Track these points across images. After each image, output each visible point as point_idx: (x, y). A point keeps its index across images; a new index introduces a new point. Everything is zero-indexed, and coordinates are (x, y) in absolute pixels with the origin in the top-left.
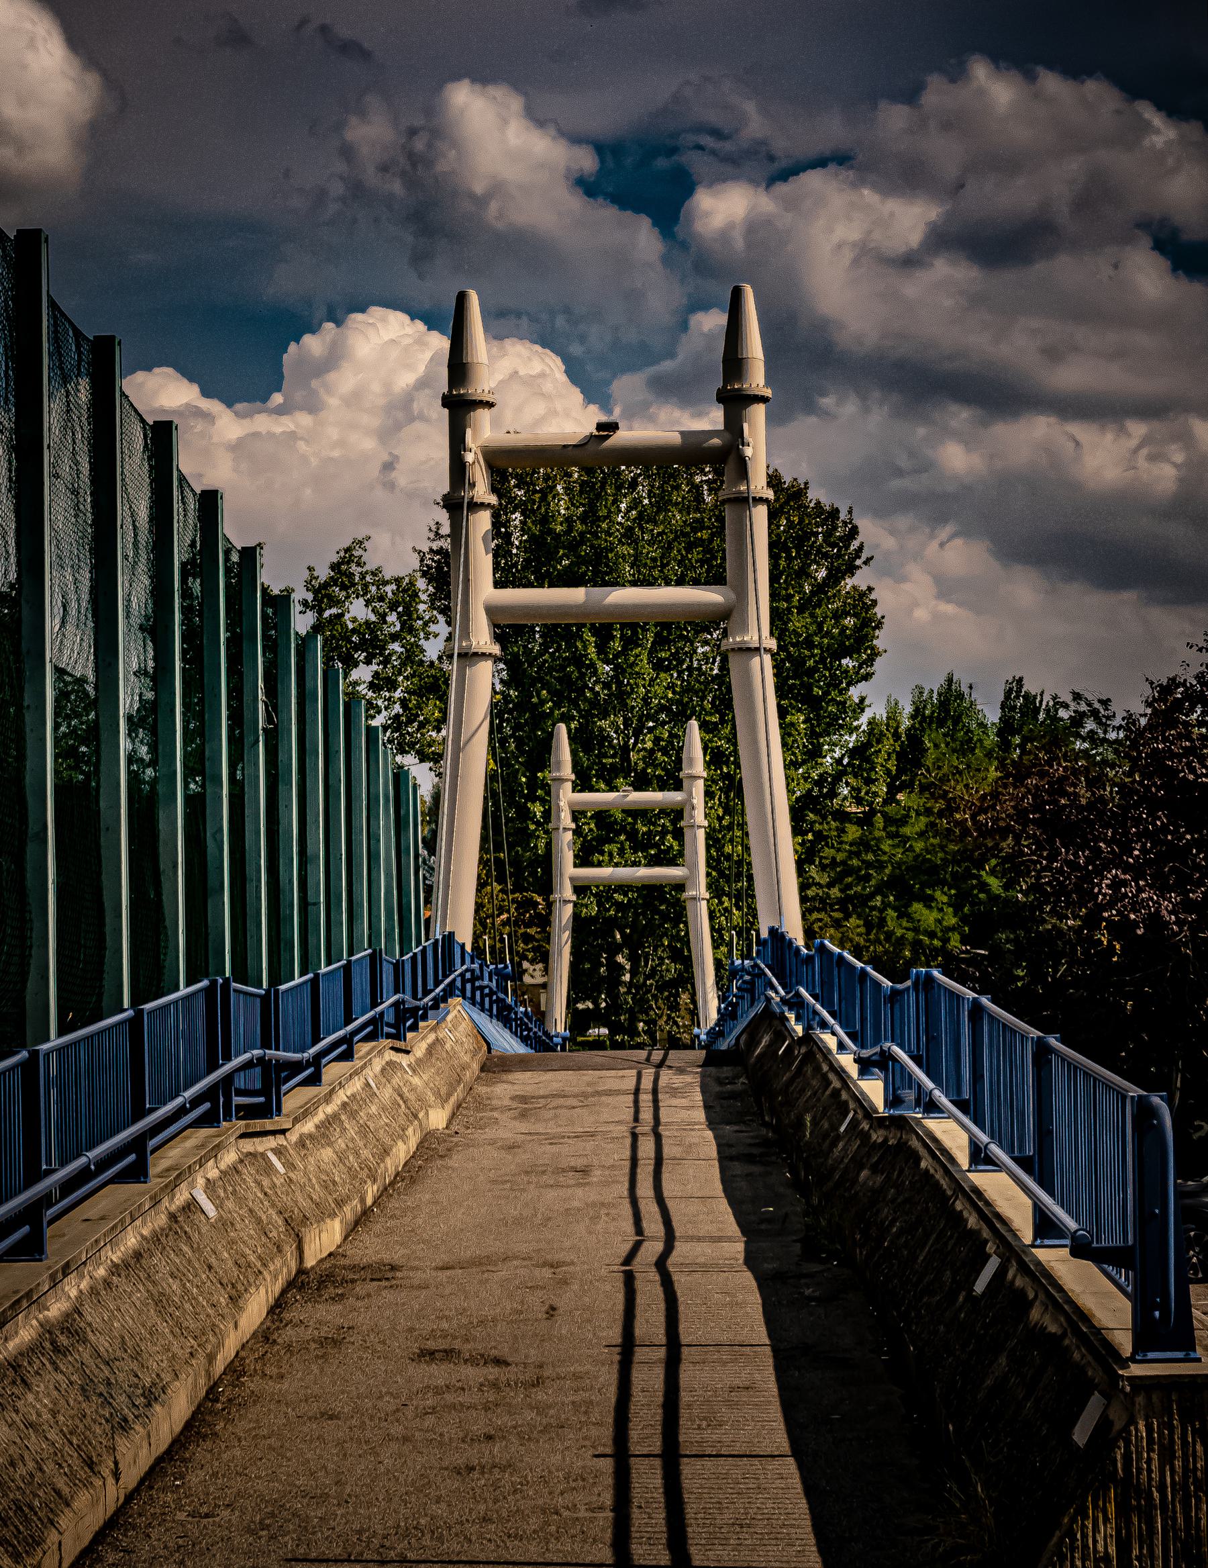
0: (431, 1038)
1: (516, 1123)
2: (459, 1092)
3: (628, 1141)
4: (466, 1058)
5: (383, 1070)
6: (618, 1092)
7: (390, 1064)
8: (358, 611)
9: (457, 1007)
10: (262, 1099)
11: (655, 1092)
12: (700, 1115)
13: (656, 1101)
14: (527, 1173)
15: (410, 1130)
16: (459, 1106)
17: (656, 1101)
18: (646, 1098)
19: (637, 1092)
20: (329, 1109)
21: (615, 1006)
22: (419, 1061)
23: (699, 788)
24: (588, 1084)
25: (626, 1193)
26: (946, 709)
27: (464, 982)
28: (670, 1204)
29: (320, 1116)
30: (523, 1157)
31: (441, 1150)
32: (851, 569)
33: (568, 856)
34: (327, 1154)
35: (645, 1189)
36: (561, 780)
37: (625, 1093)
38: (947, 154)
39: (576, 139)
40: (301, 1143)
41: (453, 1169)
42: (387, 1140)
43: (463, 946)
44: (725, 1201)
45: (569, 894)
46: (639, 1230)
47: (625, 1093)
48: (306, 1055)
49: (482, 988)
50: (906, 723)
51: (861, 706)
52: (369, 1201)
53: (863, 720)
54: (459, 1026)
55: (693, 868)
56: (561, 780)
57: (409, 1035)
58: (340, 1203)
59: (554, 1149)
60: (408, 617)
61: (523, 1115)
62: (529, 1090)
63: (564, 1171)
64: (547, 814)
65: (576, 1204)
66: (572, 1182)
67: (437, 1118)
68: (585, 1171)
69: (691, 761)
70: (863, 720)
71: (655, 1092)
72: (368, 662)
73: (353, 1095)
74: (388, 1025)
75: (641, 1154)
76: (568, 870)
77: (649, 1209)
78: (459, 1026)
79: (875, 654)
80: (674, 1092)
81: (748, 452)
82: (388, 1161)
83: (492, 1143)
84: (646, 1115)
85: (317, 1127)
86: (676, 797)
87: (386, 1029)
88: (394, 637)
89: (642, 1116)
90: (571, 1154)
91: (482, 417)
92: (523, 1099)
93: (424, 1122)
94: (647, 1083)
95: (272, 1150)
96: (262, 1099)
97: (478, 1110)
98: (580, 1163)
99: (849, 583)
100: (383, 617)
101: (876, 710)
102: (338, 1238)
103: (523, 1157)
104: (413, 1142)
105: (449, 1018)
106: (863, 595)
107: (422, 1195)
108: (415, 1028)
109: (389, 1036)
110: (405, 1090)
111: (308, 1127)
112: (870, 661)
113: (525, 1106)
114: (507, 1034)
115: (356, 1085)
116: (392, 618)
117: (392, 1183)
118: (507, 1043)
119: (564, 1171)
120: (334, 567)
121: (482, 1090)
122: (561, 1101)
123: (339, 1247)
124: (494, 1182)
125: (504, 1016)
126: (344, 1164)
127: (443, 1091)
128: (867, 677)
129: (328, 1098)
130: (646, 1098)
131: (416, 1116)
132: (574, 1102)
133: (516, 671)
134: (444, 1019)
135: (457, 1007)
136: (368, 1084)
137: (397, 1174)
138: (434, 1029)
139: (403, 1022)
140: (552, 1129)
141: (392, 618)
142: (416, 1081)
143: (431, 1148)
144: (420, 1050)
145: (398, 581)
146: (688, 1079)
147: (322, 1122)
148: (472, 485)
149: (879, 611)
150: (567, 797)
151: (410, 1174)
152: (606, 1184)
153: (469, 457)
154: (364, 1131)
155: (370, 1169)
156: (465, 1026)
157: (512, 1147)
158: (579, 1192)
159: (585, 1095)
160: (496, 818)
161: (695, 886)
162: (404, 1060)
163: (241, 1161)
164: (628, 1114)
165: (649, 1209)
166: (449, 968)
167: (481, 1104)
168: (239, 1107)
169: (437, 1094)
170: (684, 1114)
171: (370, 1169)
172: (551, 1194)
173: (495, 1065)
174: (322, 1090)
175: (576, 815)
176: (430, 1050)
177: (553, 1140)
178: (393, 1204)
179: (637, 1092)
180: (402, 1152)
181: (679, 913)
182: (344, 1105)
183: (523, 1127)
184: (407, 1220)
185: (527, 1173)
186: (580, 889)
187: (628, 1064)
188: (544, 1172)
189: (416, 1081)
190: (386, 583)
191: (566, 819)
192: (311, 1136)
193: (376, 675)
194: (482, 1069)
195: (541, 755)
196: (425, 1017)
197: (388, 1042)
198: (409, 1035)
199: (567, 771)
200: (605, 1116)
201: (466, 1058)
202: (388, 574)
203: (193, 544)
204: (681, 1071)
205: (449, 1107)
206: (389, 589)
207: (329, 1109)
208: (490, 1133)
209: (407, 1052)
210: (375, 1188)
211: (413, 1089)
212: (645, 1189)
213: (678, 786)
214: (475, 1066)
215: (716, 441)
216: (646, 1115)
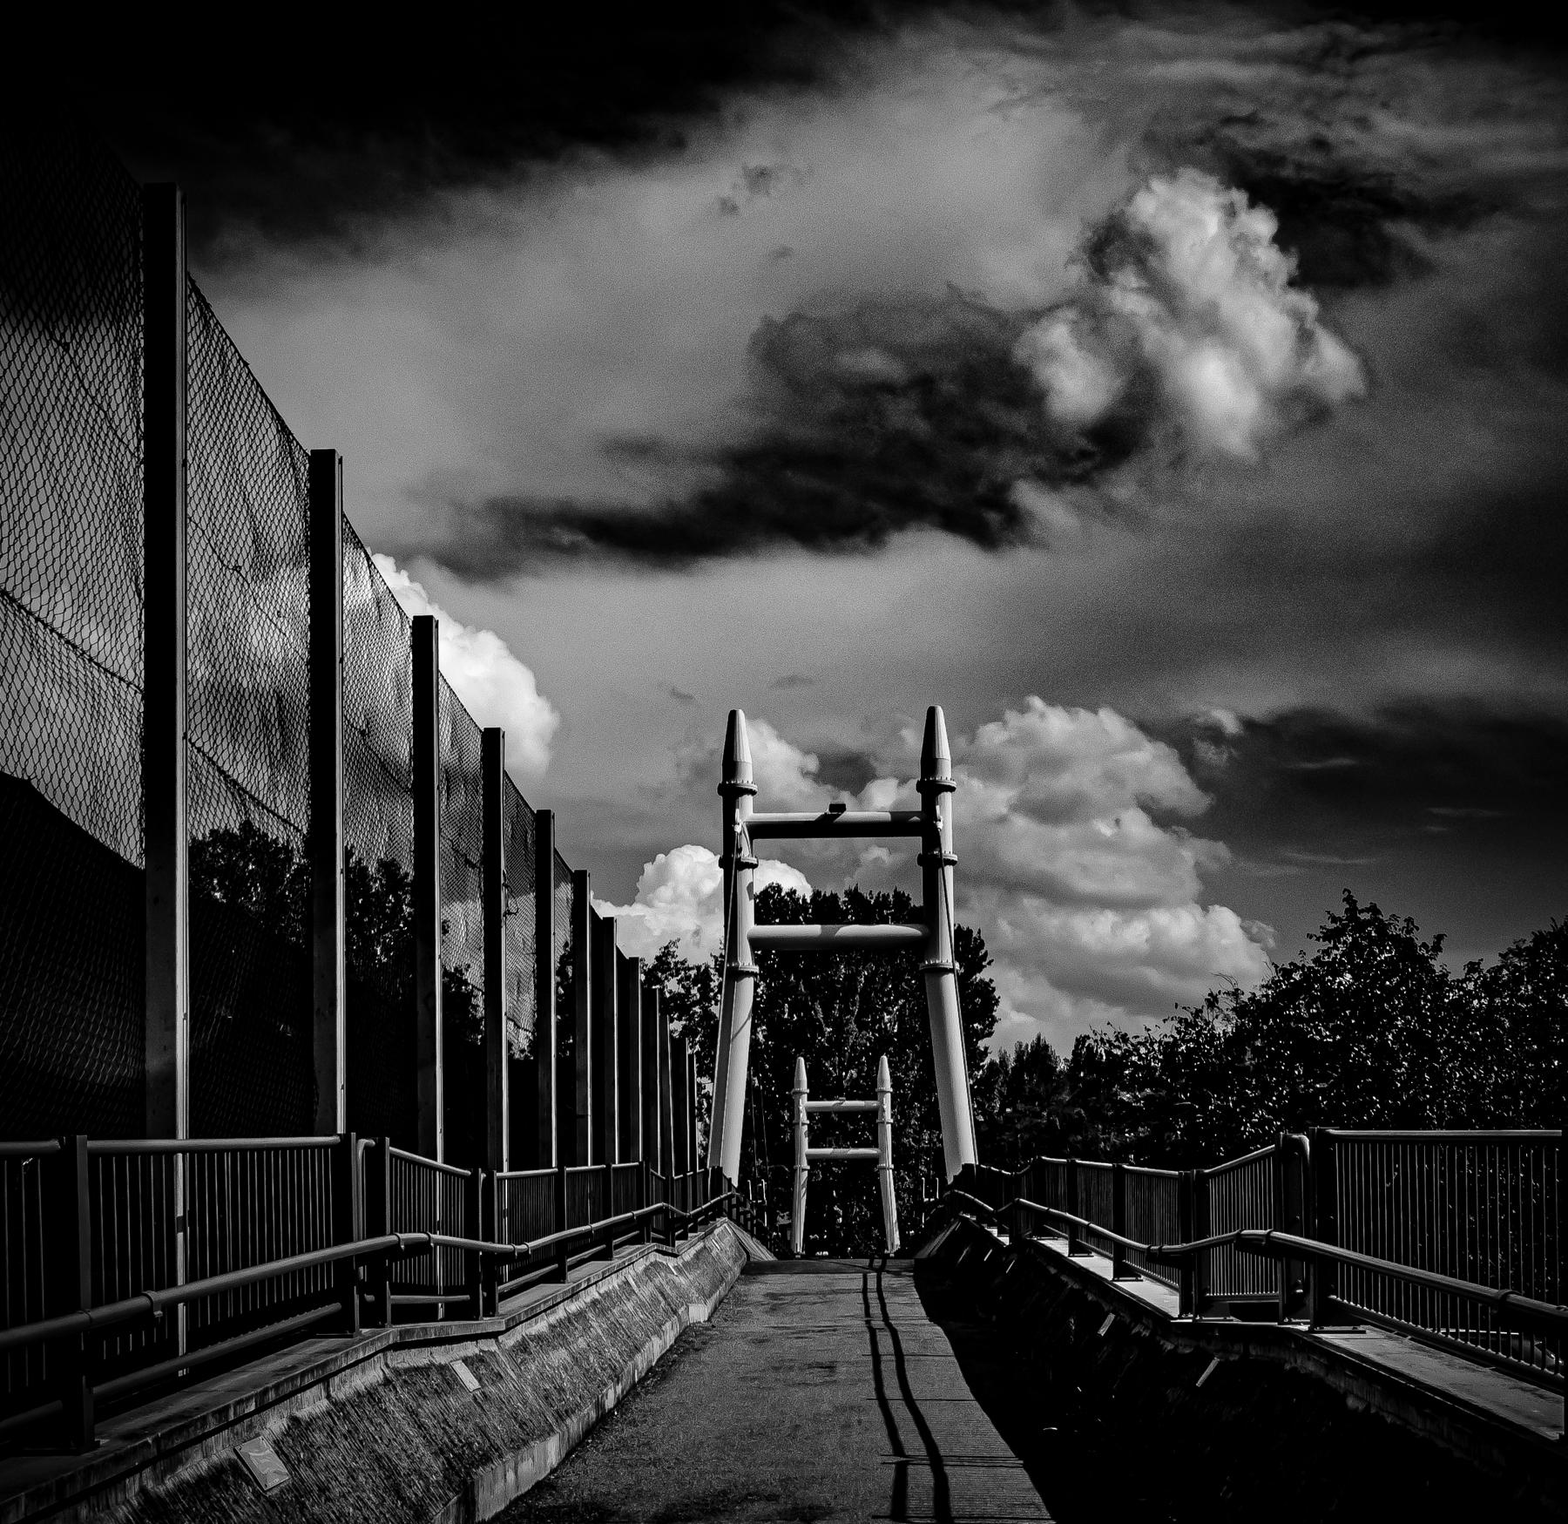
0: (700, 1245)
1: (765, 1317)
2: (721, 1291)
3: (868, 1336)
4: (730, 1263)
5: (646, 1269)
6: (849, 1291)
7: (655, 1264)
8: (673, 986)
9: (723, 1226)
10: (467, 1297)
11: (879, 1290)
12: (921, 1311)
13: (881, 1299)
14: (776, 1369)
15: (668, 1325)
16: (721, 1302)
17: (881, 1299)
18: (873, 1296)
19: (865, 1291)
20: (573, 1307)
21: (833, 1234)
22: (686, 1264)
23: (887, 1099)
24: (826, 1285)
25: (874, 1395)
26: (1038, 1055)
27: (731, 1206)
28: (922, 1408)
29: (560, 1313)
30: (771, 1351)
31: (697, 1342)
32: (980, 969)
33: (805, 1141)
34: (559, 1356)
35: (892, 1391)
36: (801, 1093)
37: (856, 1291)
38: (1016, 758)
39: (806, 752)
40: (523, 1347)
41: (706, 1364)
42: (640, 1335)
43: (730, 1180)
44: (976, 1404)
45: (805, 1165)
46: (898, 1448)
47: (856, 1291)
48: (523, 1247)
49: (745, 1213)
50: (1011, 1064)
51: (985, 1053)
52: (610, 1403)
53: (987, 1061)
54: (724, 1237)
55: (884, 1150)
56: (801, 1093)
57: (677, 1243)
58: (560, 1417)
59: (800, 1343)
60: (706, 990)
61: (773, 1309)
62: (776, 1289)
63: (810, 1366)
64: (792, 1117)
65: (825, 1407)
66: (819, 1380)
67: (699, 1313)
68: (831, 1368)
69: (883, 1082)
70: (987, 1061)
71: (879, 1290)
72: (679, 1019)
73: (608, 1294)
74: (655, 1231)
75: (881, 1350)
76: (805, 1149)
77: (901, 1412)
78: (724, 1237)
79: (994, 1020)
80: (895, 1292)
81: (940, 825)
82: (638, 1358)
83: (746, 1335)
84: (875, 1310)
85: (552, 1327)
86: (874, 1104)
87: (653, 1234)
88: (695, 1003)
89: (872, 1311)
90: (818, 1347)
91: (748, 801)
92: (773, 1296)
93: (684, 1318)
94: (872, 1284)
95: (465, 1360)
96: (467, 1297)
97: (736, 1305)
98: (825, 1358)
99: (979, 976)
100: (688, 990)
101: (993, 1057)
102: (553, 1459)
103: (771, 1351)
104: (670, 1337)
105: (716, 1231)
106: (987, 984)
107: (671, 1392)
108: (684, 1237)
109: (655, 1240)
110: (667, 1288)
111: (540, 1326)
112: (991, 1025)
113: (775, 1302)
114: (764, 1249)
115: (614, 1282)
116: (694, 991)
117: (642, 1380)
118: (763, 1254)
119: (810, 1366)
120: (657, 958)
121: (741, 1288)
122: (804, 1298)
123: (553, 1471)
124: (743, 1379)
125: (762, 1236)
126: (580, 1367)
127: (707, 1288)
128: (990, 1034)
129: (573, 1295)
130: (873, 1296)
131: (675, 1312)
132: (812, 1299)
133: (767, 973)
134: (711, 1232)
135: (723, 1226)
136: (627, 1283)
137: (650, 1369)
138: (703, 1238)
139: (669, 1231)
140: (796, 1323)
141: (694, 991)
142: (681, 1280)
143: (689, 1342)
144: (688, 1256)
145: (698, 968)
146: (904, 1281)
147: (560, 1322)
148: (740, 850)
149: (996, 994)
150: (804, 1103)
151: (663, 1370)
152: (854, 1383)
153: (738, 829)
154: (613, 1330)
155: (614, 1370)
156: (729, 1239)
157: (761, 1341)
158: (826, 1392)
159: (824, 1294)
160: (758, 1119)
161: (885, 1161)
162: (671, 1263)
163: (387, 1382)
164: (860, 1311)
165: (901, 1412)
166: (717, 1190)
167: (740, 1300)
168: (396, 1307)
169: (701, 1291)
170: (907, 1310)
171: (614, 1370)
172: (800, 1394)
173: (752, 1270)
174: (565, 1287)
175: (810, 1115)
176: (697, 1256)
177: (801, 1334)
178: (638, 1405)
179: (865, 1291)
180: (656, 1348)
181: (875, 1179)
182: (594, 1303)
183: (774, 1321)
184: (643, 1428)
185: (776, 1369)
186: (812, 1161)
187: (854, 1269)
188: (791, 1368)
189: (681, 1280)
190: (690, 969)
191: (803, 1117)
192: (539, 1338)
193: (684, 1027)
194: (743, 1272)
195: (789, 1079)
196: (694, 1230)
197: (654, 1245)
198: (677, 1243)
199: (804, 1088)
200: (841, 1312)
201: (730, 1263)
202: (690, 964)
203: (566, 945)
204: (897, 1274)
205: (711, 1303)
206: (693, 973)
207: (573, 1307)
208: (745, 1327)
209: (675, 1256)
210: (619, 1388)
211: (676, 1286)
212: (892, 1391)
213: (875, 1098)
214: (737, 1270)
215: (916, 818)
216: (875, 1310)
